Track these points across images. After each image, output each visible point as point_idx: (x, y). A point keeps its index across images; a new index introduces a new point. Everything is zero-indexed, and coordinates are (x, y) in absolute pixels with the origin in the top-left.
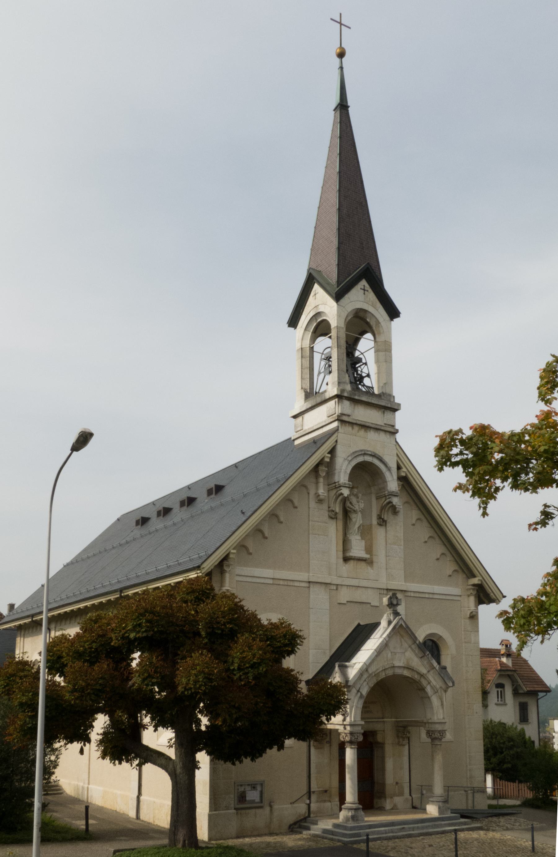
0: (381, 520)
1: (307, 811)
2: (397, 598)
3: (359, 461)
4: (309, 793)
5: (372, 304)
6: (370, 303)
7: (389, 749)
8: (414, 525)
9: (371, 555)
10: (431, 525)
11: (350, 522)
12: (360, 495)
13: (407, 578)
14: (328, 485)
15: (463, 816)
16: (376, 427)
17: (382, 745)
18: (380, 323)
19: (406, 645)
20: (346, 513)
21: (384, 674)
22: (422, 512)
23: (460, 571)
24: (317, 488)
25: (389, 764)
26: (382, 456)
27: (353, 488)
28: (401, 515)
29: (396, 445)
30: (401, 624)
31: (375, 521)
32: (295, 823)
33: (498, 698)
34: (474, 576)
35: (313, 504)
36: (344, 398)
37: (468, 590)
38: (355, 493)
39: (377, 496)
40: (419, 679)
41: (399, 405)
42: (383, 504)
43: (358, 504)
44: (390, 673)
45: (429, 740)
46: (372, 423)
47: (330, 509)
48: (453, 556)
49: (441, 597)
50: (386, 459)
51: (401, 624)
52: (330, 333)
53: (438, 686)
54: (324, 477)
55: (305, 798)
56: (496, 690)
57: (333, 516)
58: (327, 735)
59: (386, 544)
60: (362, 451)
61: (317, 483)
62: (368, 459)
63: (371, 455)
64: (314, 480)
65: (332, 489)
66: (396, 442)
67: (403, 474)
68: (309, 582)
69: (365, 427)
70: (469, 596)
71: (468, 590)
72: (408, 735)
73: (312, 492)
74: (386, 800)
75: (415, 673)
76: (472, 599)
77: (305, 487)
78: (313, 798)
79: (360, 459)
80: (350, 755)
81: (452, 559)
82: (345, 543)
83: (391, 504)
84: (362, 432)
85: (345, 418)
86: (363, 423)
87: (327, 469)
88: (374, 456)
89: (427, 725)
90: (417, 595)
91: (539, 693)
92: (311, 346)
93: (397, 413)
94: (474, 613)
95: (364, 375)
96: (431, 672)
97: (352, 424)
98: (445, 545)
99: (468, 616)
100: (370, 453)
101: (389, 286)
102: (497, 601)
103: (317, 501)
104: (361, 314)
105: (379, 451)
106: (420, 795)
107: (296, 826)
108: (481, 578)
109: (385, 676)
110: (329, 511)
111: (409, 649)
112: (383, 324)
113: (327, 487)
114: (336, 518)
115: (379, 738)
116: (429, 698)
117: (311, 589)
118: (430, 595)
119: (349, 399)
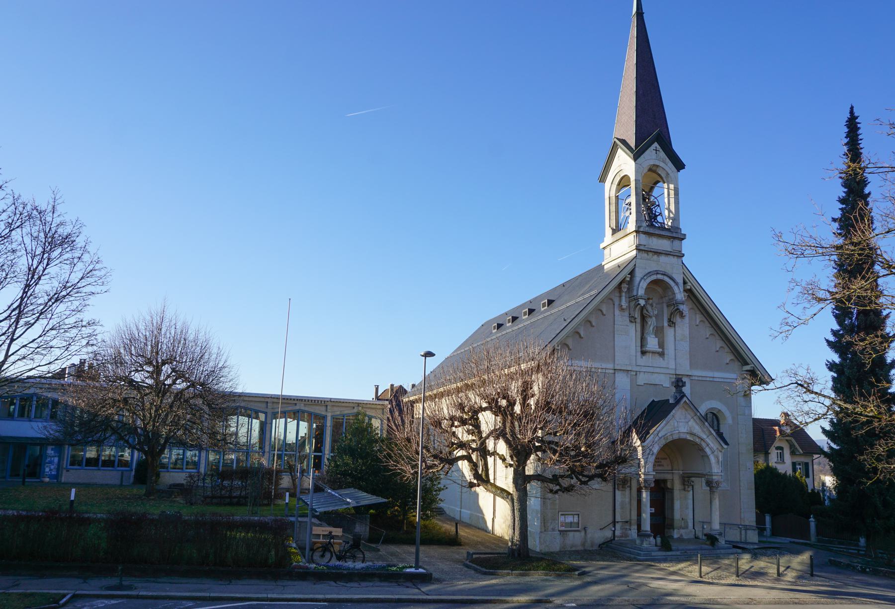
2: (682, 381)
4: (614, 522)
7: (677, 493)
9: (663, 349)
12: (654, 305)
13: (693, 365)
15: (735, 547)
17: (671, 491)
20: (644, 318)
22: (704, 315)
23: (736, 360)
24: (620, 301)
25: (677, 504)
27: (649, 299)
28: (687, 319)
31: (666, 324)
32: (603, 544)
33: (778, 458)
34: (747, 364)
35: (617, 312)
41: (685, 235)
43: (652, 311)
44: (676, 437)
45: (708, 488)
50: (675, 276)
53: (715, 448)
54: (626, 292)
55: (611, 526)
56: (776, 451)
57: (632, 319)
61: (620, 297)
62: (660, 277)
63: (662, 274)
64: (617, 294)
66: (683, 263)
69: (657, 253)
72: (692, 484)
73: (617, 303)
77: (611, 299)
78: (618, 526)
79: (654, 277)
80: (645, 495)
83: (678, 311)
85: (642, 248)
88: (657, 273)
89: (706, 477)
95: (657, 214)
104: (654, 168)
105: (669, 271)
107: (605, 546)
108: (753, 366)
110: (630, 317)
112: (671, 174)
113: (628, 299)
115: (669, 485)
116: (708, 456)
117: (616, 375)
119: (645, 233)
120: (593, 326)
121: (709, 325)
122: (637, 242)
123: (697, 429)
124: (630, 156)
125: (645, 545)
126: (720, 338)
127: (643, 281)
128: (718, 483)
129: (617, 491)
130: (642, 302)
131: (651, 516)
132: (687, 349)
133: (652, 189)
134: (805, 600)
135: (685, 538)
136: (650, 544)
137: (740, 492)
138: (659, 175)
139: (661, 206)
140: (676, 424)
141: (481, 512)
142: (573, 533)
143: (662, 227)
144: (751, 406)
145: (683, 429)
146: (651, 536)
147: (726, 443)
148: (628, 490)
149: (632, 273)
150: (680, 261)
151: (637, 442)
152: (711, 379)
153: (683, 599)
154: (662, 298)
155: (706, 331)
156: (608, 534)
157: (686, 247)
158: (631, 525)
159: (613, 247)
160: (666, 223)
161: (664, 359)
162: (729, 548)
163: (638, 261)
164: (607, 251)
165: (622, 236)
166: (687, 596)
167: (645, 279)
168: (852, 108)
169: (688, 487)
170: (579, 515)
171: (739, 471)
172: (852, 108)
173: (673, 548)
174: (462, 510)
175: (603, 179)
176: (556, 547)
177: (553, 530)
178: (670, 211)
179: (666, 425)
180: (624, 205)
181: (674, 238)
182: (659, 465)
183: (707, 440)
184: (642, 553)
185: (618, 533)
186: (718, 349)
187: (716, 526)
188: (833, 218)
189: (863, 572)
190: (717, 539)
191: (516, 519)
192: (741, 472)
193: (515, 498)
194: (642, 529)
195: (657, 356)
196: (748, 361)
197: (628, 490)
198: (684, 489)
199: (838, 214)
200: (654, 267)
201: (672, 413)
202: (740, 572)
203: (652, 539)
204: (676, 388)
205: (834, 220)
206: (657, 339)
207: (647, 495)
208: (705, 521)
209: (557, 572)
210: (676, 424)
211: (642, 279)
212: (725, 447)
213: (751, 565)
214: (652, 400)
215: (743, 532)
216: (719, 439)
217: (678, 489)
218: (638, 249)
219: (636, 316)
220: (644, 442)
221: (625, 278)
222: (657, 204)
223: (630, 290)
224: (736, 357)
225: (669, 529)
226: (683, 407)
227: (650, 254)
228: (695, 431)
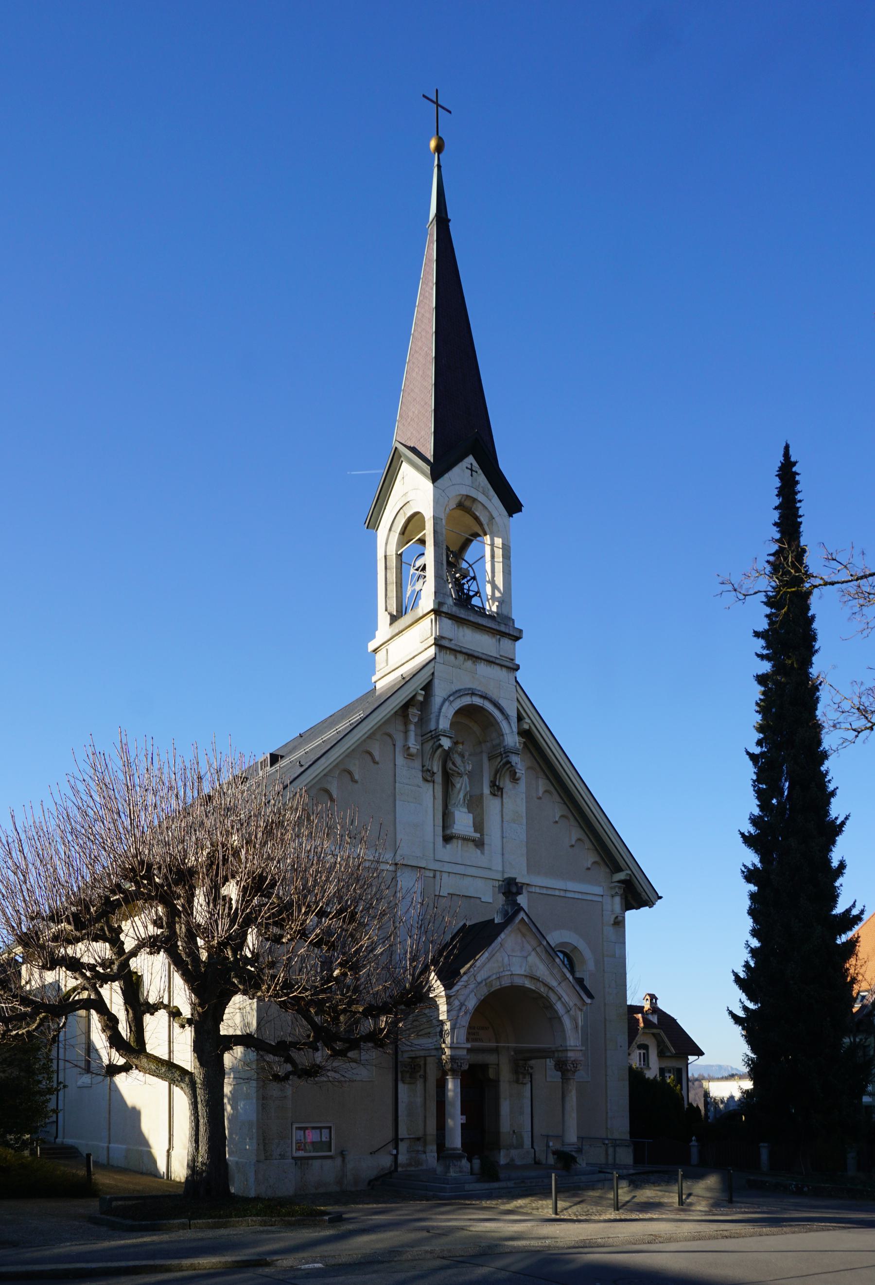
0: (496, 788)
1: (393, 1164)
3: (464, 704)
5: (483, 491)
6: (481, 489)
7: (505, 1087)
9: (482, 835)
10: (563, 800)
11: (452, 790)
12: (467, 754)
13: (532, 867)
14: (422, 736)
16: (489, 658)
17: (496, 1083)
18: (494, 518)
19: (528, 948)
21: (498, 984)
24: (406, 739)
25: (505, 1107)
26: (497, 699)
28: (522, 786)
29: (516, 686)
30: (523, 918)
31: (486, 791)
32: (377, 1179)
33: (640, 1061)
34: (619, 869)
35: (400, 760)
36: (443, 615)
37: (612, 888)
39: (490, 755)
42: (498, 766)
43: (460, 764)
44: (506, 982)
46: (483, 654)
47: (425, 768)
48: (593, 844)
49: (577, 896)
50: (503, 703)
52: (424, 529)
53: (571, 1004)
54: (416, 724)
57: (428, 776)
58: (420, 1067)
59: (502, 821)
60: (469, 689)
61: (406, 732)
63: (481, 696)
64: (401, 727)
65: (427, 741)
66: (517, 682)
67: (526, 727)
70: (613, 896)
71: (612, 888)
72: (530, 1071)
73: (399, 743)
74: (500, 1152)
76: (617, 900)
78: (403, 1147)
79: (467, 700)
80: (452, 1085)
82: (447, 817)
83: (509, 765)
84: (469, 663)
85: (445, 643)
86: (471, 652)
87: (420, 713)
88: (484, 697)
90: (544, 891)
91: (690, 1057)
92: (399, 553)
93: (518, 643)
94: (620, 918)
95: (471, 593)
96: (563, 984)
97: (455, 652)
98: (581, 827)
99: (612, 922)
100: (479, 693)
101: (506, 465)
102: (651, 903)
104: (468, 503)
106: (545, 1148)
108: (629, 872)
109: (499, 987)
110: (423, 771)
111: (533, 953)
112: (498, 519)
113: (420, 738)
114: (434, 782)
115: (491, 1074)
116: (559, 1019)
120: (356, 782)
122: (436, 632)
123: (542, 970)
124: (423, 473)
125: (452, 1174)
126: (576, 824)
127: (447, 703)
128: (575, 1063)
129: (401, 1086)
130: (446, 743)
131: (462, 1129)
132: (523, 837)
133: (466, 543)
134: (738, 1231)
136: (461, 1172)
138: (477, 519)
139: (478, 578)
140: (506, 959)
141: (145, 1143)
142: (320, 1161)
143: (481, 612)
144: (624, 943)
145: (518, 969)
146: (463, 1157)
147: (590, 996)
148: (420, 1085)
149: (428, 687)
150: (511, 676)
151: (438, 989)
152: (562, 894)
153: (534, 1243)
154: (480, 743)
155: (555, 809)
156: (386, 1161)
157: (521, 652)
158: (425, 1144)
159: (392, 646)
160: (488, 608)
161: (483, 853)
163: (439, 670)
164: (380, 656)
165: (408, 624)
166: (540, 1238)
167: (451, 702)
168: (787, 448)
169: (524, 1078)
170: (330, 1128)
171: (606, 1050)
172: (787, 448)
174: (106, 1145)
175: (373, 522)
176: (287, 1188)
177: (282, 1156)
178: (494, 587)
179: (489, 959)
180: (412, 571)
181: (503, 634)
183: (560, 991)
184: (448, 1186)
185: (402, 1158)
186: (573, 843)
187: (572, 1137)
188: (755, 632)
189: (799, 1192)
191: (201, 1121)
193: (198, 1081)
194: (447, 1145)
195: (471, 845)
196: (622, 864)
197: (420, 1085)
198: (517, 1081)
199: (763, 625)
200: (467, 682)
201: (499, 939)
202: (620, 1205)
203: (464, 1162)
204: (507, 897)
205: (757, 634)
206: (471, 815)
207: (455, 1086)
209: (286, 1218)
210: (506, 959)
211: (445, 701)
212: (588, 1001)
213: (633, 1194)
214: (461, 924)
215: (611, 1150)
216: (578, 988)
218: (439, 643)
219: (435, 770)
220: (451, 989)
221: (414, 696)
222: (472, 574)
223: (423, 721)
226: (519, 929)
227: (461, 658)
228: (538, 974)
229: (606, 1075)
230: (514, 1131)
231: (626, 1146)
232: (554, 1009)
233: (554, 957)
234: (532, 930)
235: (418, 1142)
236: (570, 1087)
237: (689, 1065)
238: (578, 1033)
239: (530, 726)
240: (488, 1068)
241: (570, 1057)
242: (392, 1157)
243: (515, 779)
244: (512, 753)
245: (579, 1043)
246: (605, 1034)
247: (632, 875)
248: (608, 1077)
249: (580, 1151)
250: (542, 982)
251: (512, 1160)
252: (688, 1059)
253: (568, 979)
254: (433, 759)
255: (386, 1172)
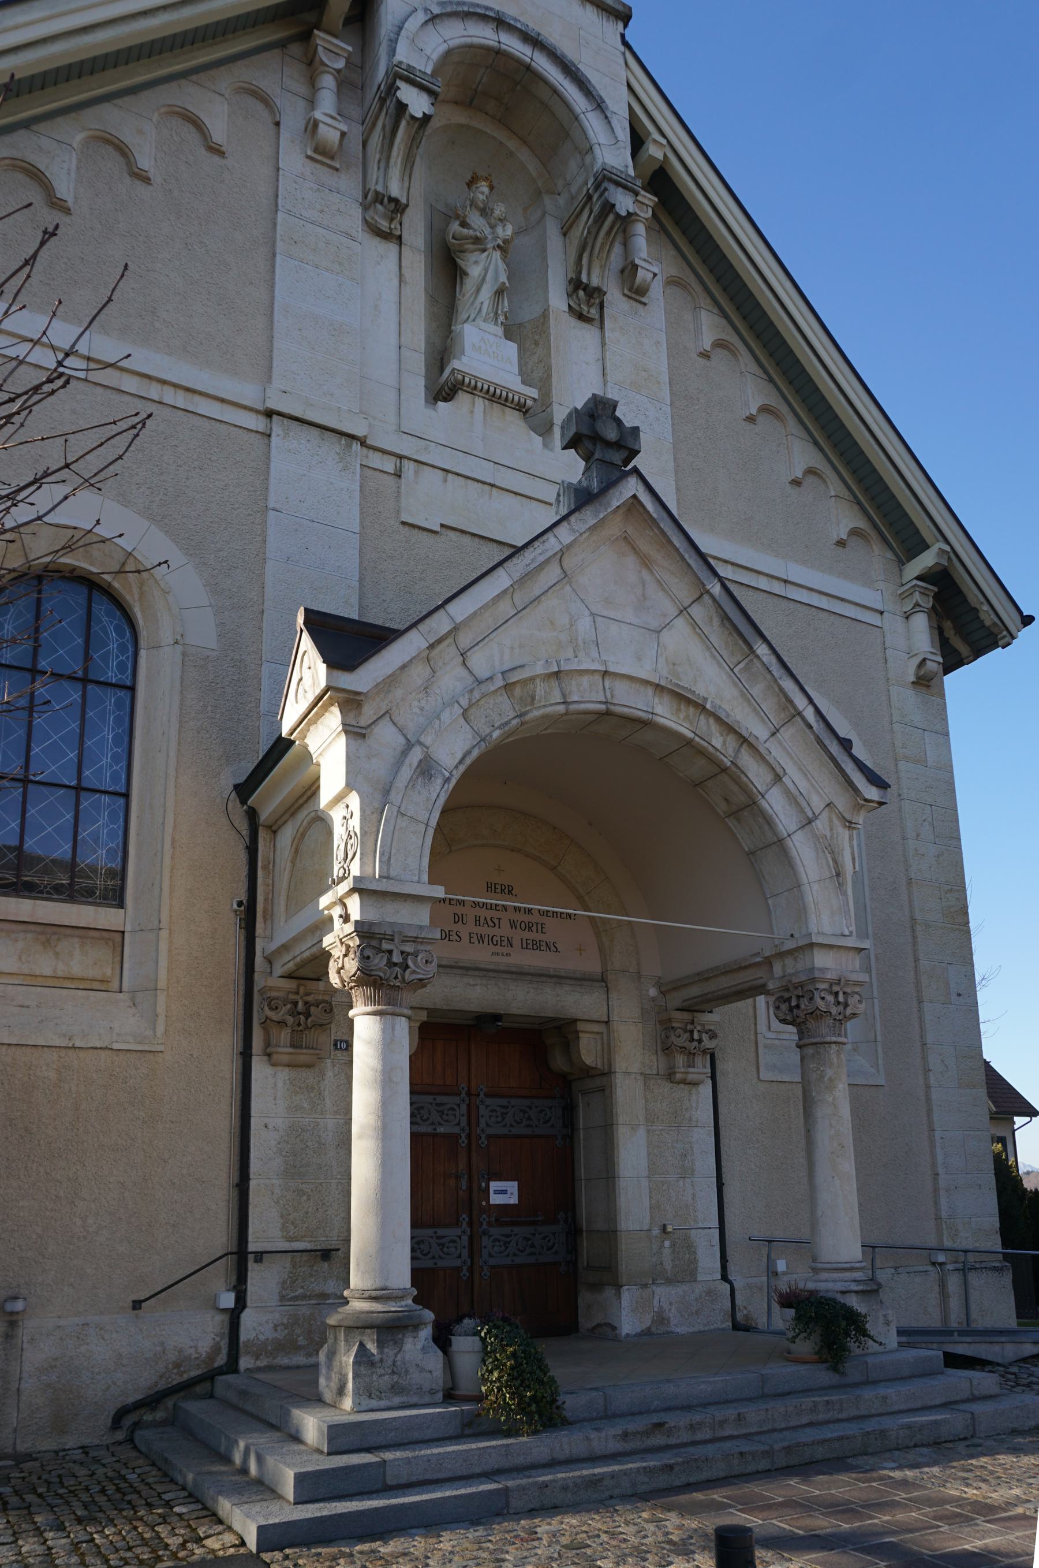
0: (581, 293)
1: (224, 1344)
8: (705, 355)
10: (766, 372)
24: (312, 103)
29: (624, 54)
30: (634, 496)
31: (558, 300)
32: (152, 1401)
38: (481, 197)
40: (730, 752)
49: (815, 600)
51: (634, 496)
53: (817, 803)
68: (269, 414)
72: (707, 1043)
73: (293, 120)
75: (714, 726)
81: (846, 493)
88: (535, 42)
91: (1016, 1119)
96: (786, 734)
99: (912, 679)
103: (310, 153)
109: (561, 708)
111: (680, 623)
115: (589, 1053)
116: (779, 844)
118: (775, 583)
121: (754, 367)
128: (838, 987)
129: (259, 1069)
135: (681, 1330)
137: (928, 1100)
140: (584, 624)
162: (926, 1373)
171: (920, 1002)
173: (571, 1403)
182: (536, 946)
183: (776, 753)
186: (799, 474)
190: (855, 1323)
192: (927, 1006)
195: (513, 417)
198: (670, 1076)
204: (587, 458)
208: (779, 1234)
210: (584, 624)
212: (872, 793)
217: (635, 1068)
224: (875, 526)
225: (597, 1287)
229: (927, 1071)
230: (664, 1228)
231: (995, 1268)
232: (763, 813)
233: (750, 640)
234: (670, 542)
235: (326, 1264)
236: (829, 1073)
237: (1016, 1132)
238: (844, 893)
239: (665, 155)
240: (577, 1032)
241: (822, 970)
242: (220, 1318)
243: (637, 293)
244: (618, 184)
245: (847, 925)
246: (916, 960)
247: (952, 556)
248: (931, 1074)
249: (872, 1290)
250: (718, 719)
251: (661, 1319)
252: (1014, 1123)
253: (800, 714)
254: (387, 167)
255: (194, 1373)
